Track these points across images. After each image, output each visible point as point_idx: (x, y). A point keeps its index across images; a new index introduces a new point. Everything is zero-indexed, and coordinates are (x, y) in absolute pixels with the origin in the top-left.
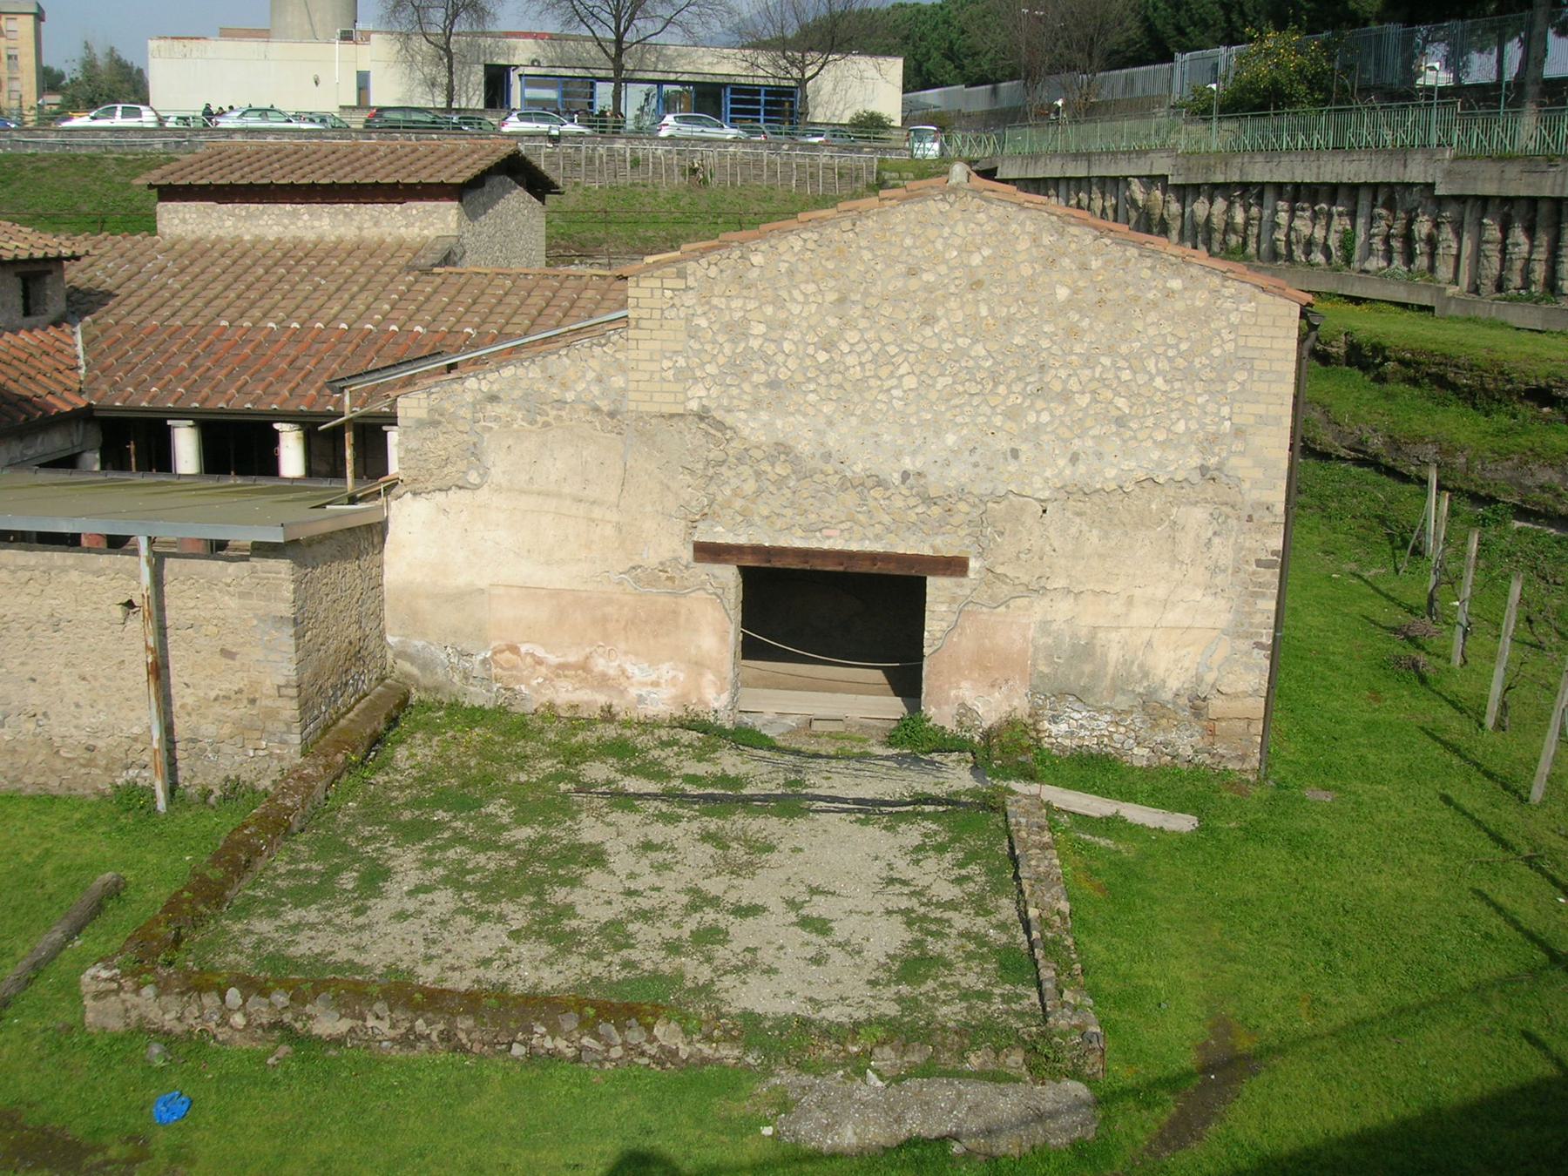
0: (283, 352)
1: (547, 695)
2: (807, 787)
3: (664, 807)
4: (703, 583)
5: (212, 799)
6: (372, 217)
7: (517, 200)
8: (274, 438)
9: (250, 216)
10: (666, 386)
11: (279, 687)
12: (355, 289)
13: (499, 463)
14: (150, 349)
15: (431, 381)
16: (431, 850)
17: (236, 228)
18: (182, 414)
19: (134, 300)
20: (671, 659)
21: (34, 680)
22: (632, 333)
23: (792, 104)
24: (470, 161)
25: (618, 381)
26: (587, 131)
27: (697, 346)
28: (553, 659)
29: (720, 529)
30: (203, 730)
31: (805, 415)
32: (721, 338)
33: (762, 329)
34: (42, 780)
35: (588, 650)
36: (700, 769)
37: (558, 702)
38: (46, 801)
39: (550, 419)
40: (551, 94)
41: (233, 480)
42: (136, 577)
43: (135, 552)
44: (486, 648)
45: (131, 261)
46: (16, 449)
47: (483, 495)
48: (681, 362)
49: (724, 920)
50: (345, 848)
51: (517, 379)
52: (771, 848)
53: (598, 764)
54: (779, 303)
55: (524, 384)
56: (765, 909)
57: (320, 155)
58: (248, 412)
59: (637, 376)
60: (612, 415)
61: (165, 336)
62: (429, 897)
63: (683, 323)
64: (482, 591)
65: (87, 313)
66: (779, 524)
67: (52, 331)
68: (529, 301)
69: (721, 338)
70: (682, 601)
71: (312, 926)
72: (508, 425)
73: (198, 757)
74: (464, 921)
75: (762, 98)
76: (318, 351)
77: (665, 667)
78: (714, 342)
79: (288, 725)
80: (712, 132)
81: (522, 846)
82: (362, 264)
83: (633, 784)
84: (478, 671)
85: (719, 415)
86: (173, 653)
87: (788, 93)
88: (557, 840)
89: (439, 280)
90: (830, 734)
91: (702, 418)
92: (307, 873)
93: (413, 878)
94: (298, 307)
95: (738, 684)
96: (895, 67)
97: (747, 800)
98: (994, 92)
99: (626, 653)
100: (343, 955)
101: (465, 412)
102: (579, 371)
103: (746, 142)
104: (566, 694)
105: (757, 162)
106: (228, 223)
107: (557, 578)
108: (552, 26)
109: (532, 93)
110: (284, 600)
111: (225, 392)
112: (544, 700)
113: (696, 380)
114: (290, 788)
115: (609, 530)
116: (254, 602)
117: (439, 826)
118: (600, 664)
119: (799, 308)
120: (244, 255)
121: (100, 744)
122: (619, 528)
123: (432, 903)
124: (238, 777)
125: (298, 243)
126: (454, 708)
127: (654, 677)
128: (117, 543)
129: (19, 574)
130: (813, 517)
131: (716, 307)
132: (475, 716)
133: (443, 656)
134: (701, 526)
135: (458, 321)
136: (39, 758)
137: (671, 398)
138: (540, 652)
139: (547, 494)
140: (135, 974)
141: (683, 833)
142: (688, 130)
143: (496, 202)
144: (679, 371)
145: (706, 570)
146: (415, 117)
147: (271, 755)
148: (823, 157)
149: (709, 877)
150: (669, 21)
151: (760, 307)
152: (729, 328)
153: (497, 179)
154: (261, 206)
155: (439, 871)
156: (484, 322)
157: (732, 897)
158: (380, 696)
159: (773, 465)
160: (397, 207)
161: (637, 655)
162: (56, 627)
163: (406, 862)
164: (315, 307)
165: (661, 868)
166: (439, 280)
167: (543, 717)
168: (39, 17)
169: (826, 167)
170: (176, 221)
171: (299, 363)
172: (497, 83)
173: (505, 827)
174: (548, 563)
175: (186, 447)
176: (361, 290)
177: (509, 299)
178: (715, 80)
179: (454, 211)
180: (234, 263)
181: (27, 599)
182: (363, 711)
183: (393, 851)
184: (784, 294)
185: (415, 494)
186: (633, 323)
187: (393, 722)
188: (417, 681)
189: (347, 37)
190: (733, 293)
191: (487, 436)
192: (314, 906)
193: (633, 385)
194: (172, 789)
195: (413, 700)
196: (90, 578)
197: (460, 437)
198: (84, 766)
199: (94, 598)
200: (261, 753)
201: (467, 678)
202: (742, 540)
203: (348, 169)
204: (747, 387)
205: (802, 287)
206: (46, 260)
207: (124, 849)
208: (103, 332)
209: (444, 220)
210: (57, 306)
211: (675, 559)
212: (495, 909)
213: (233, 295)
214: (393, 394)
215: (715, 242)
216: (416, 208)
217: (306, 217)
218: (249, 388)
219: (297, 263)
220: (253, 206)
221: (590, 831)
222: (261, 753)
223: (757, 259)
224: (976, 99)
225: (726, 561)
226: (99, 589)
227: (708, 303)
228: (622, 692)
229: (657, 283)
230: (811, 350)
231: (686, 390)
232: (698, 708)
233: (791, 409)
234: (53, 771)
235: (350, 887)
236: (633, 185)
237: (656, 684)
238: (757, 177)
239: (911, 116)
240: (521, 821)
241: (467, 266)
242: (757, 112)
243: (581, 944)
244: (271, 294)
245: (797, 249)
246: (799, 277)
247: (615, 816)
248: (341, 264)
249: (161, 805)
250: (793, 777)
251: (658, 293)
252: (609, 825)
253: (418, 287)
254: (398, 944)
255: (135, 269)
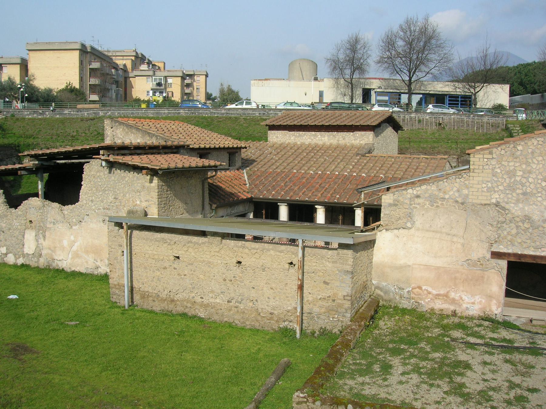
0: (316, 181)
1: (431, 305)
2: (538, 345)
3: (486, 349)
4: (494, 266)
5: (316, 335)
6: (342, 137)
7: (389, 131)
8: (315, 210)
9: (300, 136)
10: (484, 194)
11: (344, 296)
12: (339, 161)
13: (419, 220)
14: (270, 179)
15: (395, 190)
16: (404, 359)
17: (295, 140)
18: (283, 201)
19: (262, 163)
20: (480, 294)
21: (254, 288)
22: (471, 174)
23: (470, 101)
24: (376, 118)
25: (465, 192)
26: (401, 110)
27: (496, 179)
28: (434, 292)
29: (502, 247)
30: (314, 310)
31: (537, 205)
32: (505, 177)
33: (521, 173)
34: (253, 323)
35: (448, 289)
36: (495, 336)
37: (435, 308)
38: (255, 331)
39: (439, 204)
40: (386, 98)
41: (298, 224)
42: (296, 254)
43: (298, 246)
44: (410, 286)
45: (260, 150)
46: (229, 210)
47: (412, 231)
48: (490, 185)
49: (525, 394)
50: (371, 356)
51: (427, 190)
52: (533, 367)
53: (455, 331)
54: (528, 164)
55: (429, 192)
56: (540, 390)
57: (322, 116)
58: (307, 201)
59: (473, 190)
60: (462, 204)
61: (275, 175)
62: (410, 376)
63: (491, 171)
64: (409, 266)
65: (247, 167)
66: (525, 245)
67: (236, 171)
68: (401, 166)
69: (505, 177)
70: (486, 273)
71: (369, 384)
72: (423, 206)
73: (311, 319)
74: (425, 386)
75: (460, 99)
76: (329, 182)
77: (477, 297)
78: (503, 178)
79: (346, 310)
80: (445, 111)
81: (438, 360)
82: (340, 152)
83: (472, 340)
84: (406, 295)
85: (503, 204)
86: (305, 281)
87: (469, 97)
88: (450, 359)
89: (368, 158)
90: (540, 326)
91: (497, 206)
92: (360, 364)
93: (401, 369)
94: (320, 167)
95: (506, 305)
96: (507, 87)
97: (517, 348)
98: (542, 96)
99: (463, 291)
100: (383, 395)
101: (407, 201)
102: (452, 188)
103: (457, 114)
104: (438, 305)
105: (462, 121)
106: (292, 138)
107: (439, 262)
108: (386, 76)
109: (380, 98)
110: (349, 265)
111: (298, 194)
112: (430, 307)
113: (495, 191)
114: (349, 333)
115: (459, 246)
116: (338, 265)
117: (404, 351)
118: (452, 295)
119: (536, 165)
120: (298, 149)
121: (276, 312)
122: (463, 245)
123: (411, 379)
124: (325, 328)
125: (317, 145)
126: (396, 308)
127: (473, 301)
128: (293, 242)
129: (252, 250)
130: (538, 243)
131: (503, 165)
132: (404, 311)
133: (393, 289)
134: (494, 245)
135: (377, 173)
136: (253, 316)
137: (485, 198)
138: (430, 289)
139: (436, 232)
140: (313, 396)
141: (497, 358)
142: (437, 110)
143: (383, 132)
144: (489, 188)
145: (494, 262)
146: (342, 105)
147: (338, 320)
148: (485, 119)
149: (513, 376)
150: (428, 73)
151: (520, 165)
152: (508, 173)
153: (384, 125)
154: (304, 133)
155: (410, 367)
156: (386, 173)
157: (525, 385)
158: (371, 302)
159: (523, 224)
160: (352, 133)
161: (467, 292)
162: (264, 270)
163: (396, 361)
164: (326, 167)
165: (493, 372)
166: (368, 158)
167: (430, 314)
168: (207, 76)
169: (487, 123)
170: (274, 137)
171: (322, 185)
172: (366, 94)
173: (429, 353)
174: (435, 257)
175: (284, 212)
176: (341, 161)
177: (394, 165)
178: (443, 93)
179: (371, 135)
180: (295, 151)
181: (254, 260)
182: (367, 307)
183: (390, 358)
184: (530, 161)
185: (387, 230)
186: (472, 171)
187: (376, 312)
188: (382, 297)
189: (316, 79)
190: (510, 160)
191: (415, 210)
192: (367, 377)
193: (471, 193)
194: (301, 330)
195: (381, 304)
196: (278, 253)
197: (404, 210)
198: (269, 320)
199: (279, 261)
200: (335, 319)
201: (401, 297)
202: (510, 251)
203: (334, 120)
204: (514, 194)
205: (537, 158)
206: (237, 148)
207: (287, 350)
208: (254, 173)
209: (368, 138)
210: (239, 164)
211: (484, 257)
212: (436, 383)
213: (297, 162)
214: (380, 194)
215: (502, 142)
216: (358, 134)
217: (319, 136)
218: (306, 193)
219: (318, 151)
220: (301, 133)
221: (462, 356)
222: (335, 319)
223: (520, 148)
224: (536, 99)
225: (503, 259)
226: (281, 258)
227: (500, 163)
228: (460, 306)
229: (481, 156)
230: (539, 181)
231: (491, 195)
232: (489, 313)
233: (531, 203)
234: (257, 321)
235: (378, 370)
236: (418, 129)
237: (473, 303)
238: (462, 126)
239: (512, 106)
240: (435, 351)
241: (375, 153)
242: (458, 104)
243: (472, 398)
244: (310, 162)
245: (535, 144)
246: (536, 154)
247: (469, 351)
248: (333, 152)
249: (298, 335)
250: (531, 341)
251: (482, 160)
252: (468, 354)
253: (361, 161)
254: (402, 392)
255: (261, 152)
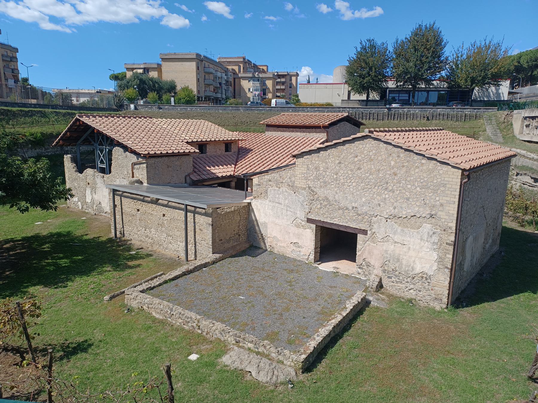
22: (296, 168)
85: (313, 188)
204: (319, 182)
